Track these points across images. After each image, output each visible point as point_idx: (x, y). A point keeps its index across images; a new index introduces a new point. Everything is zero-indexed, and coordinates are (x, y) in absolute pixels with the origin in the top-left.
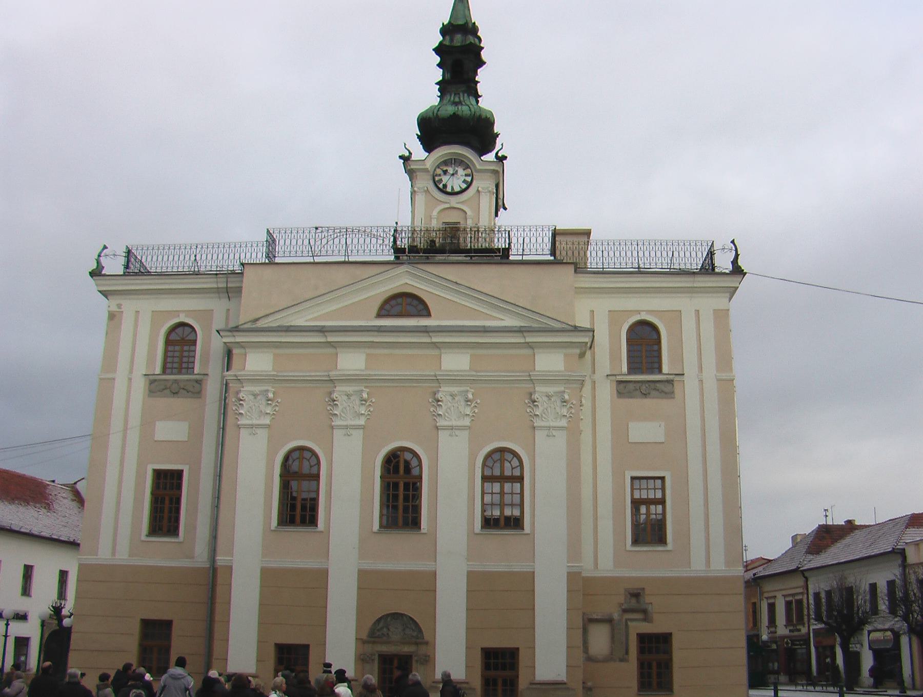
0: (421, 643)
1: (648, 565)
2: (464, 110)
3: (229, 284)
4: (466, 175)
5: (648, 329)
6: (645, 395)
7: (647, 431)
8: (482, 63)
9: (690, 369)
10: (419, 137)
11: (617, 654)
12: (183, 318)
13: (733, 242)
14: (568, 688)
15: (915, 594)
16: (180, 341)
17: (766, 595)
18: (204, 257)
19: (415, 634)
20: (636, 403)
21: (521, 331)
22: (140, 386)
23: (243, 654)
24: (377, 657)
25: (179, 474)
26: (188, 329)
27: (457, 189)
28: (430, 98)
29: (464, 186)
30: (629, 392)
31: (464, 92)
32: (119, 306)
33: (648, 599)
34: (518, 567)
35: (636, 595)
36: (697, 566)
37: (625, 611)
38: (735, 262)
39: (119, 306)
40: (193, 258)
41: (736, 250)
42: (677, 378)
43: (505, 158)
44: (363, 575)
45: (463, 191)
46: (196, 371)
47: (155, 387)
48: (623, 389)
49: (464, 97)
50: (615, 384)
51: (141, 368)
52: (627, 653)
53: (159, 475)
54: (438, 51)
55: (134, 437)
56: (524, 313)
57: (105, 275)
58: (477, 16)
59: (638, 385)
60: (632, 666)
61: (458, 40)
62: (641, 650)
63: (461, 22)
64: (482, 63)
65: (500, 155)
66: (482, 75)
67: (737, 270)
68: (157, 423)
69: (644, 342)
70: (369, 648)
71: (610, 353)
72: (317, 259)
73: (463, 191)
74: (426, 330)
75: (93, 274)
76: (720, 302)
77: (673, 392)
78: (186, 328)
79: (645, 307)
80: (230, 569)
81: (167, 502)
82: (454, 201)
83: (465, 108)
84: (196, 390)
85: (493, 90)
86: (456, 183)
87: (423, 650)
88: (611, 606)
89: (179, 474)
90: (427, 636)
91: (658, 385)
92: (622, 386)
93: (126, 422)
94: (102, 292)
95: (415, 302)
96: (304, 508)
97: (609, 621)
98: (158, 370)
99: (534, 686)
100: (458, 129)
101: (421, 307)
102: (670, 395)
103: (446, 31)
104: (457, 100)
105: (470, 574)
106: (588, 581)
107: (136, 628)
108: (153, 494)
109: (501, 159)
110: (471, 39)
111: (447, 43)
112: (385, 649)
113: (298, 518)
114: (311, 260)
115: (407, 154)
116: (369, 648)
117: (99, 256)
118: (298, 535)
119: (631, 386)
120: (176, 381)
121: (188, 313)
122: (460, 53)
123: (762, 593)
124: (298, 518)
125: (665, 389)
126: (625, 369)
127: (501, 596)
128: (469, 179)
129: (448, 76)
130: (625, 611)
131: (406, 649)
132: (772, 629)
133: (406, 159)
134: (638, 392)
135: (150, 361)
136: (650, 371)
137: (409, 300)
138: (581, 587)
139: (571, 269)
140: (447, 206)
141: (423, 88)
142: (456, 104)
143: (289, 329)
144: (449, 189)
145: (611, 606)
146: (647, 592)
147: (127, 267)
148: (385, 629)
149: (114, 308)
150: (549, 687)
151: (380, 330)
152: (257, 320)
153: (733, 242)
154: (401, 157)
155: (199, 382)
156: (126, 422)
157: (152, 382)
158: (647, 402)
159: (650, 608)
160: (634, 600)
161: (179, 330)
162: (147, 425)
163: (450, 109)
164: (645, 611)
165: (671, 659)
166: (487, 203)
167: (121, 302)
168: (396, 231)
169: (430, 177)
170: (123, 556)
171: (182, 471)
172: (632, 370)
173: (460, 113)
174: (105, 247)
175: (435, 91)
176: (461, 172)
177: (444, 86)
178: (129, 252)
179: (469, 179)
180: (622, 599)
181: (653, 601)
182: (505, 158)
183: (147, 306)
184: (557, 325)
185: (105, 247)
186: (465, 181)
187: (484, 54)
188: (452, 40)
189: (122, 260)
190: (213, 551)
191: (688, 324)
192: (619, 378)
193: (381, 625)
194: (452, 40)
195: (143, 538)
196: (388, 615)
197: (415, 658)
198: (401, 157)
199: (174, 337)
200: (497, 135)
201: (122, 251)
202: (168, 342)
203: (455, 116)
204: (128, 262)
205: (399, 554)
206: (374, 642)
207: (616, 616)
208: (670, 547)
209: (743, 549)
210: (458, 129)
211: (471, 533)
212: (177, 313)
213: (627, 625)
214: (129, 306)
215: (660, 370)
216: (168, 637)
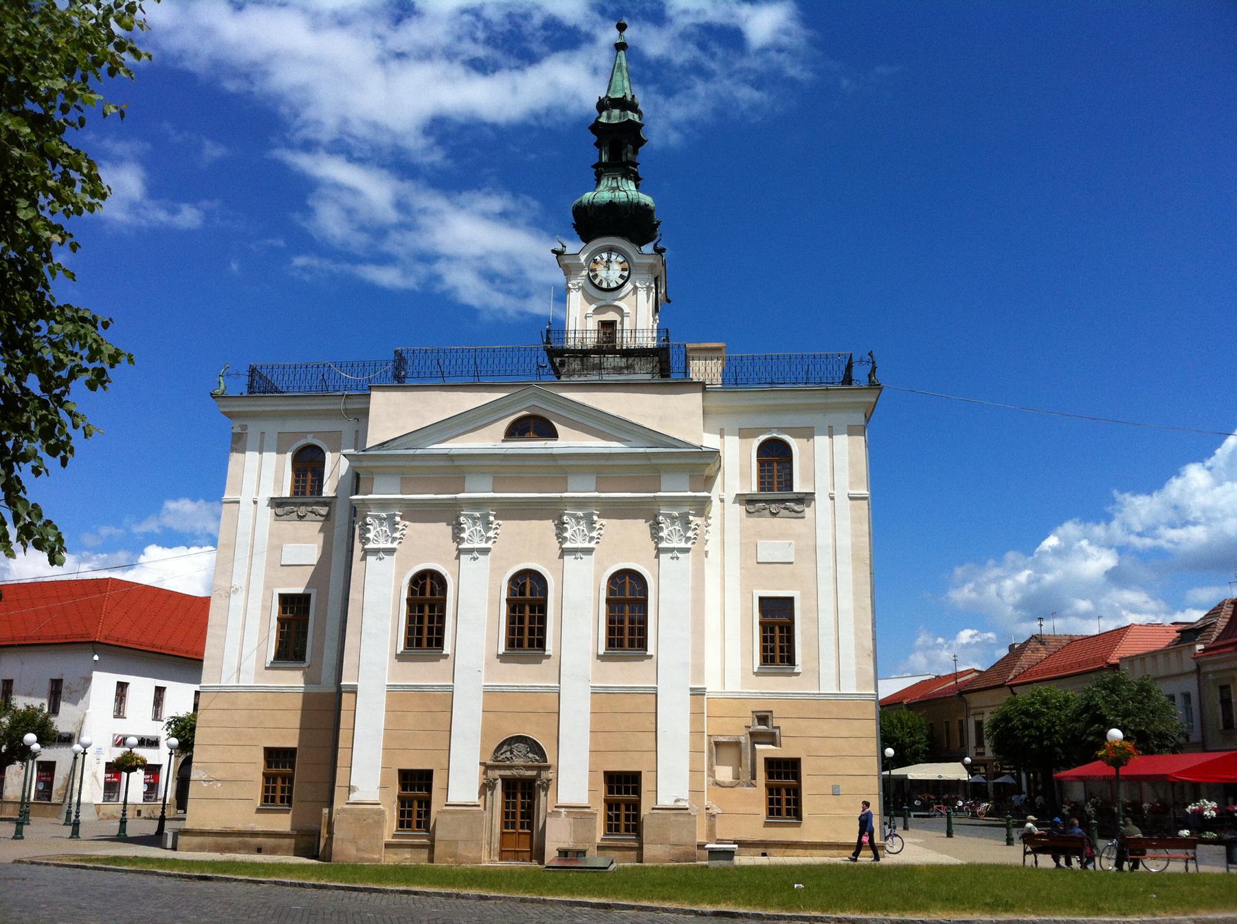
4: (623, 270)
10: (575, 226)
15: (416, 787)
17: (972, 712)
20: (766, 522)
27: (613, 285)
29: (621, 282)
35: (763, 719)
36: (828, 687)
39: (244, 427)
40: (320, 377)
52: (754, 777)
60: (759, 793)
61: (616, 116)
62: (770, 774)
72: (449, 382)
83: (622, 194)
90: (550, 760)
96: (771, 483)
104: (615, 185)
121: (317, 434)
123: (968, 709)
128: (626, 274)
132: (980, 750)
135: (278, 482)
139: (700, 388)
140: (603, 303)
144: (604, 285)
147: (251, 387)
149: (238, 430)
158: (776, 520)
162: (275, 548)
168: (548, 331)
170: (248, 680)
173: (617, 200)
178: (253, 371)
186: (621, 277)
188: (609, 117)
189: (245, 380)
196: (512, 738)
198: (553, 251)
201: (245, 370)
204: (252, 382)
207: (743, 740)
213: (753, 749)
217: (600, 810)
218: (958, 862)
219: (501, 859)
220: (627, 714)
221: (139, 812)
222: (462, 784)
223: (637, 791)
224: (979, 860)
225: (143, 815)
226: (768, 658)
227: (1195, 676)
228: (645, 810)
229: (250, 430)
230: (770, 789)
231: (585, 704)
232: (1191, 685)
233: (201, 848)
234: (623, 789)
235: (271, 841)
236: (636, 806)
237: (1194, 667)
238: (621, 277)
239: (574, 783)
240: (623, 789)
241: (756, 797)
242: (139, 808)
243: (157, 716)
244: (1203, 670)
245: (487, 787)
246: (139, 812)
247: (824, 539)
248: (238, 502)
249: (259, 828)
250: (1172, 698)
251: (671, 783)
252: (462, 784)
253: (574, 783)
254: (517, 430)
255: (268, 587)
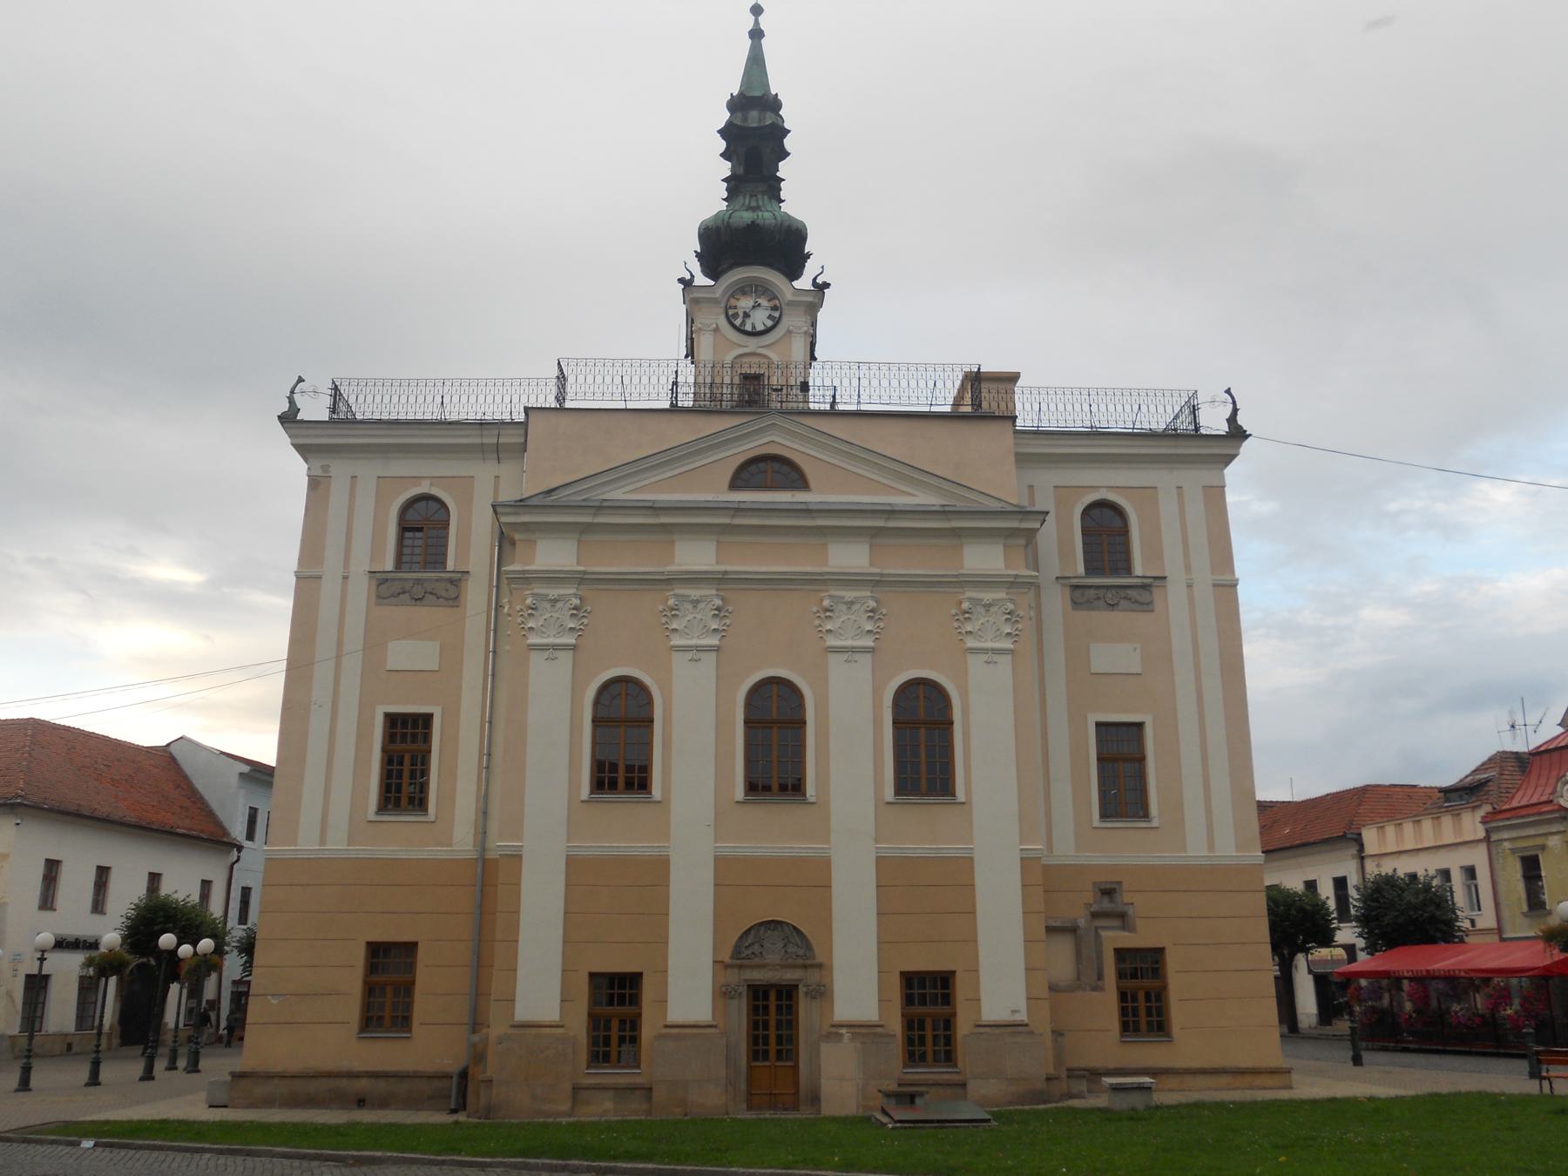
0: (812, 966)
1: (1124, 850)
2: (765, 217)
3: (497, 440)
5: (1108, 512)
6: (1112, 606)
7: (1114, 655)
8: (784, 154)
9: (1172, 567)
10: (698, 255)
11: (1086, 977)
12: (424, 488)
13: (1228, 391)
14: (1032, 1033)
15: (616, 999)
16: (422, 525)
18: (456, 399)
19: (801, 952)
20: (1099, 618)
21: (943, 513)
22: (361, 589)
23: (541, 989)
24: (743, 990)
25: (427, 719)
26: (434, 505)
27: (760, 328)
28: (711, 200)
29: (770, 323)
30: (1089, 601)
31: (763, 193)
32: (325, 468)
33: (1127, 898)
34: (950, 847)
35: (1108, 892)
36: (1195, 850)
37: (1095, 915)
38: (1232, 420)
39: (325, 468)
41: (1234, 403)
42: (1157, 583)
43: (827, 285)
44: (722, 863)
45: (767, 331)
46: (450, 565)
47: (386, 588)
48: (1080, 595)
49: (763, 200)
50: (1067, 591)
51: (361, 565)
52: (1100, 977)
53: (395, 722)
54: (724, 133)
55: (353, 666)
56: (945, 485)
57: (302, 421)
58: (777, 84)
59: (1101, 593)
60: (1108, 1000)
61: (754, 118)
63: (757, 93)
64: (784, 154)
65: (819, 281)
66: (784, 169)
67: (1237, 434)
68: (390, 645)
69: (1106, 531)
70: (733, 977)
71: (1062, 546)
72: (630, 405)
73: (767, 331)
74: (807, 511)
75: (283, 419)
76: (1204, 476)
77: (1151, 603)
78: (431, 503)
79: (1104, 483)
80: (516, 858)
81: (407, 761)
82: (752, 344)
84: (451, 592)
85: (801, 192)
86: (760, 319)
87: (813, 977)
88: (1076, 910)
89: (427, 719)
91: (1129, 592)
92: (1078, 593)
93: (340, 644)
94: (298, 447)
95: (785, 469)
97: (1073, 930)
98: (389, 565)
99: (982, 1030)
100: (752, 248)
101: (794, 475)
102: (1147, 606)
103: (735, 105)
104: (754, 204)
105: (880, 861)
106: (1048, 870)
107: (359, 956)
108: (384, 750)
109: (821, 288)
110: (769, 119)
111: (738, 122)
112: (758, 976)
113: (621, 782)
114: (621, 405)
115: (688, 277)
116: (733, 977)
117: (292, 392)
118: (621, 810)
119: (1092, 592)
120: (418, 581)
122: (755, 139)
124: (621, 782)
125: (1143, 594)
126: (1081, 570)
127: (925, 892)
128: (776, 314)
129: (741, 171)
130: (1095, 915)
131: (789, 976)
133: (687, 283)
134: (1101, 603)
136: (1115, 571)
137: (776, 466)
138: (1042, 879)
141: (704, 188)
142: (749, 208)
143: (601, 508)
144: (748, 327)
145: (1076, 910)
146: (1125, 887)
147: (333, 410)
148: (756, 946)
150: (997, 1031)
151: (739, 510)
152: (550, 492)
153: (1228, 391)
154: (681, 280)
155: (453, 582)
156: (340, 644)
157: (381, 582)
158: (1117, 616)
159: (1131, 911)
160: (1106, 900)
161: (421, 505)
162: (374, 646)
163: (747, 217)
164: (1122, 916)
165: (1165, 988)
166: (798, 349)
167: (326, 462)
169: (722, 310)
170: (337, 843)
171: (388, 716)
172: (1091, 569)
173: (760, 222)
174: (301, 380)
175: (722, 190)
176: (764, 302)
177: (735, 186)
179: (776, 314)
180: (1089, 897)
181: (1134, 900)
182: (827, 285)
183: (369, 471)
184: (996, 506)
185: (301, 380)
186: (770, 317)
187: (788, 143)
189: (328, 401)
190: (482, 833)
191: (1167, 507)
192: (1074, 581)
193: (750, 940)
194: (745, 119)
195: (372, 817)
196: (761, 924)
197: (802, 989)
198: (681, 280)
199: (411, 515)
200: (808, 256)
201: (326, 388)
202: (405, 528)
203: (753, 227)
205: (773, 833)
206: (741, 967)
207: (1082, 922)
208: (1155, 823)
209: (513, 1015)
210: (752, 248)
211: (880, 804)
212: (417, 479)
213: (1097, 936)
214: (340, 470)
215: (1128, 570)
216: (411, 967)
217: (896, 1026)
218: (1411, 1093)
219: (750, 1108)
220: (925, 892)
221: (70, 1046)
222: (688, 990)
223: (635, 1000)
224: (1463, 1088)
225: (75, 1049)
226: (1109, 811)
227: (1483, 848)
228: (963, 1027)
229: (333, 472)
230: (1123, 996)
231: (707, 875)
232: (1478, 858)
233: (267, 1102)
234: (928, 999)
235: (382, 1086)
236: (949, 1023)
237: (1481, 834)
238: (770, 317)
239: (857, 988)
240: (928, 999)
241: (1103, 1006)
242: (69, 1039)
243: (98, 906)
244: (1494, 837)
245: (723, 994)
246: (70, 1046)
247: (1180, 642)
248: (320, 577)
249: (357, 1066)
250: (1446, 874)
251: (1000, 987)
252: (688, 990)
253: (857, 988)
254: (745, 475)
255: (365, 707)
